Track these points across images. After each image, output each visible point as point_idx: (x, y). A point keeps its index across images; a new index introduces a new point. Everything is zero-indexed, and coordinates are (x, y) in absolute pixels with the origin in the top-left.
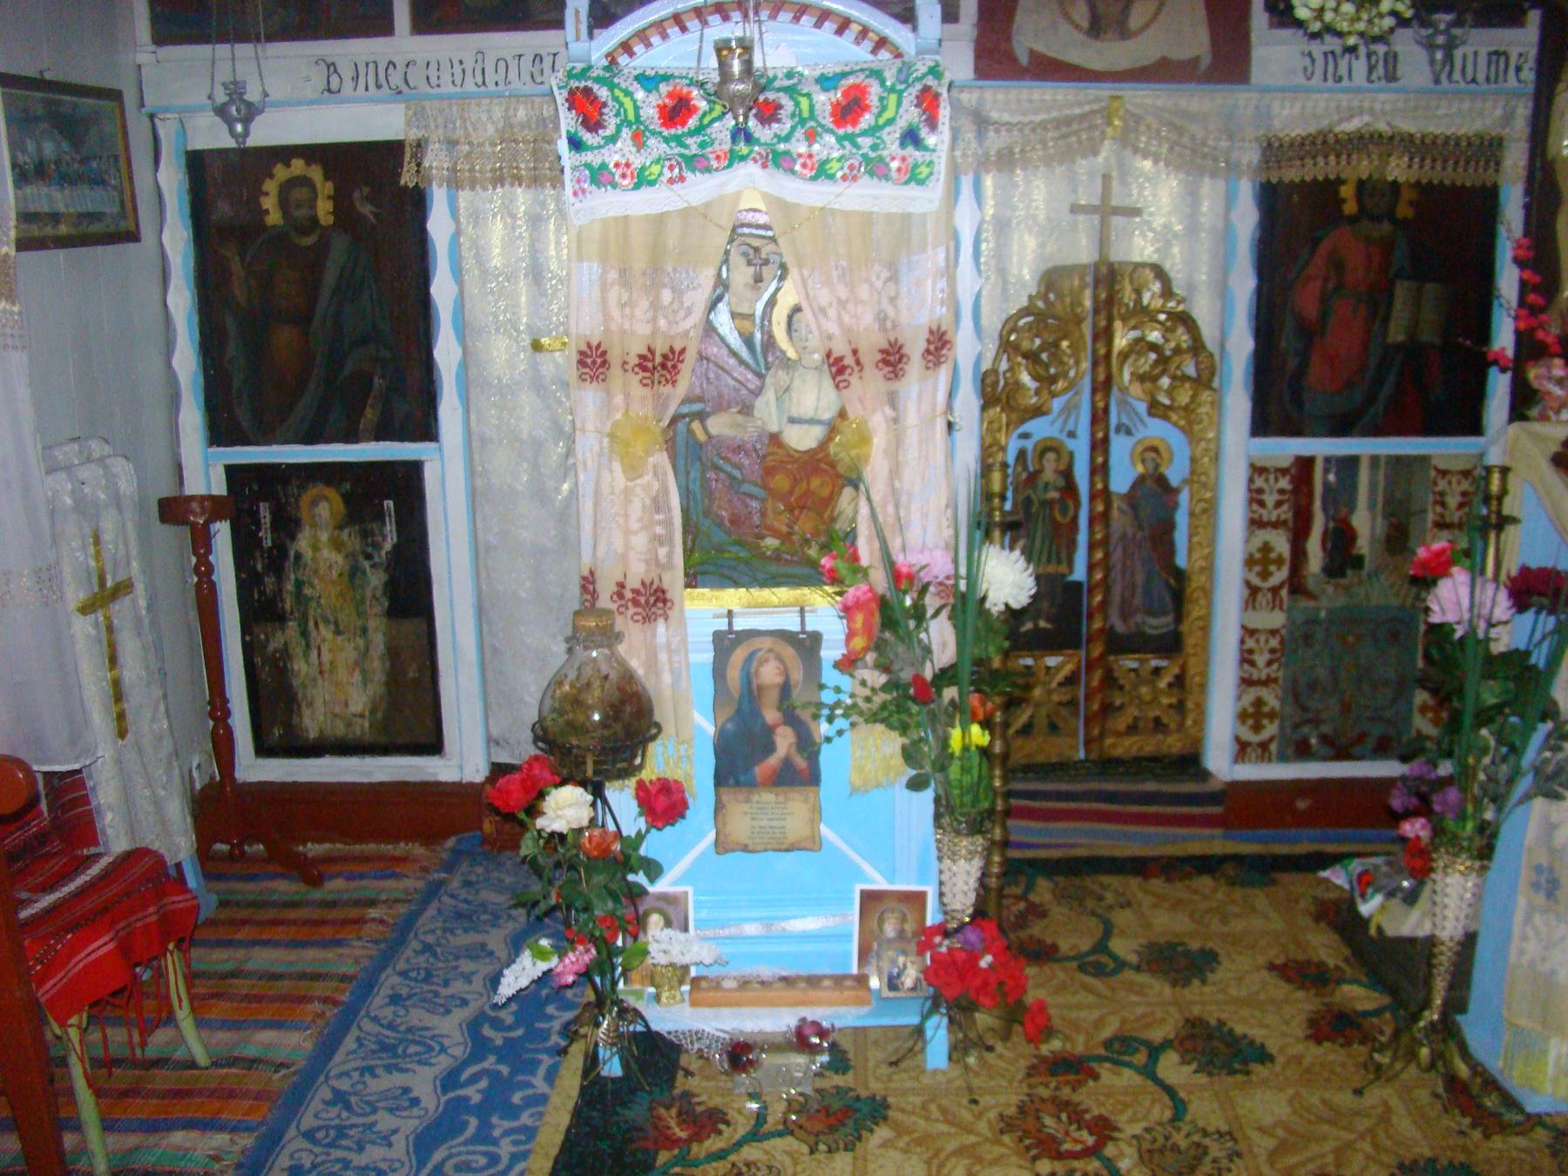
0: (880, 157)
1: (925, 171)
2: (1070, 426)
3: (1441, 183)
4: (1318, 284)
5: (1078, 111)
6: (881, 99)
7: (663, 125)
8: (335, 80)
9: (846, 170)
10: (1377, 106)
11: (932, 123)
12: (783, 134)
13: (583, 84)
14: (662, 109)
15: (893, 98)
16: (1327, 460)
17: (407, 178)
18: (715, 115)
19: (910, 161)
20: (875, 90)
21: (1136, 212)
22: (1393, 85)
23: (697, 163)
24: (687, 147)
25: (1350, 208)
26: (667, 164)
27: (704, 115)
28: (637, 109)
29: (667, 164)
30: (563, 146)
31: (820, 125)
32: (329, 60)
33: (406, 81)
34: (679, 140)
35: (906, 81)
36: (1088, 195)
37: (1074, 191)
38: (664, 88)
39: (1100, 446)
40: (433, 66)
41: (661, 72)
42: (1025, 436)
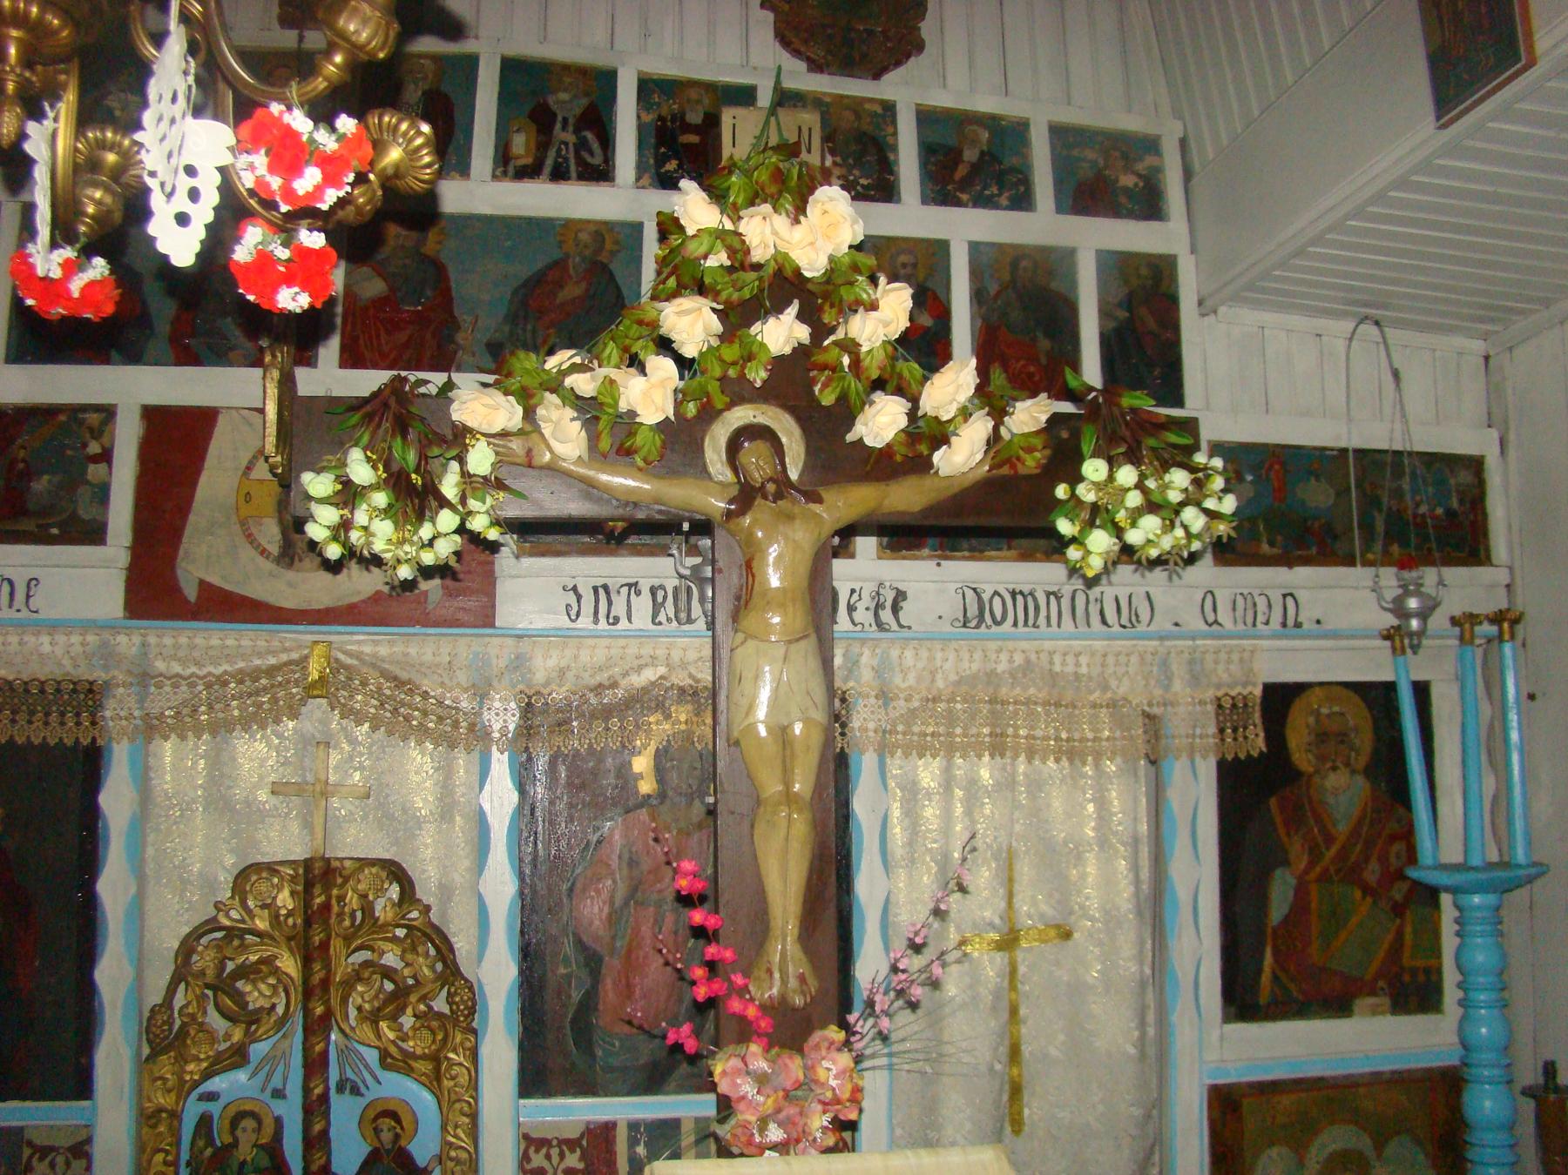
2: (276, 1081)
16: (633, 1126)
39: (316, 1107)
42: (211, 1097)
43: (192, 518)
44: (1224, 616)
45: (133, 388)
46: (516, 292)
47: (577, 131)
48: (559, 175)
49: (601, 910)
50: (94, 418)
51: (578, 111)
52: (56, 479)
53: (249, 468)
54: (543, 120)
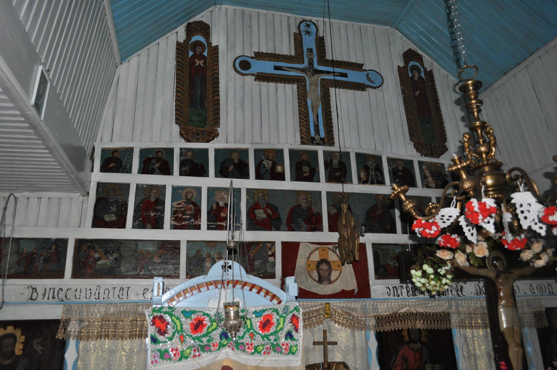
0: (278, 343)
1: (295, 349)
3: (434, 329)
4: (400, 366)
5: (315, 308)
6: (278, 320)
7: (192, 332)
8: (35, 295)
9: (265, 350)
10: (410, 304)
11: (297, 330)
12: (241, 336)
13: (159, 314)
14: (192, 324)
15: (282, 319)
17: (60, 335)
18: (213, 327)
19: (289, 345)
20: (275, 318)
21: (335, 343)
22: (415, 297)
23: (205, 348)
24: (202, 342)
25: (407, 339)
26: (193, 349)
27: (209, 327)
28: (181, 325)
29: (193, 349)
30: (148, 340)
31: (255, 331)
32: (34, 287)
33: (66, 297)
34: (198, 338)
35: (286, 313)
36: (319, 338)
37: (314, 336)
38: (193, 316)
40: (78, 291)
41: (192, 309)
43: (296, 271)
44: (535, 291)
45: (279, 237)
46: (367, 212)
47: (375, 172)
48: (372, 183)
49: (481, 366)
50: (269, 245)
51: (374, 167)
52: (261, 261)
53: (309, 258)
54: (366, 169)
